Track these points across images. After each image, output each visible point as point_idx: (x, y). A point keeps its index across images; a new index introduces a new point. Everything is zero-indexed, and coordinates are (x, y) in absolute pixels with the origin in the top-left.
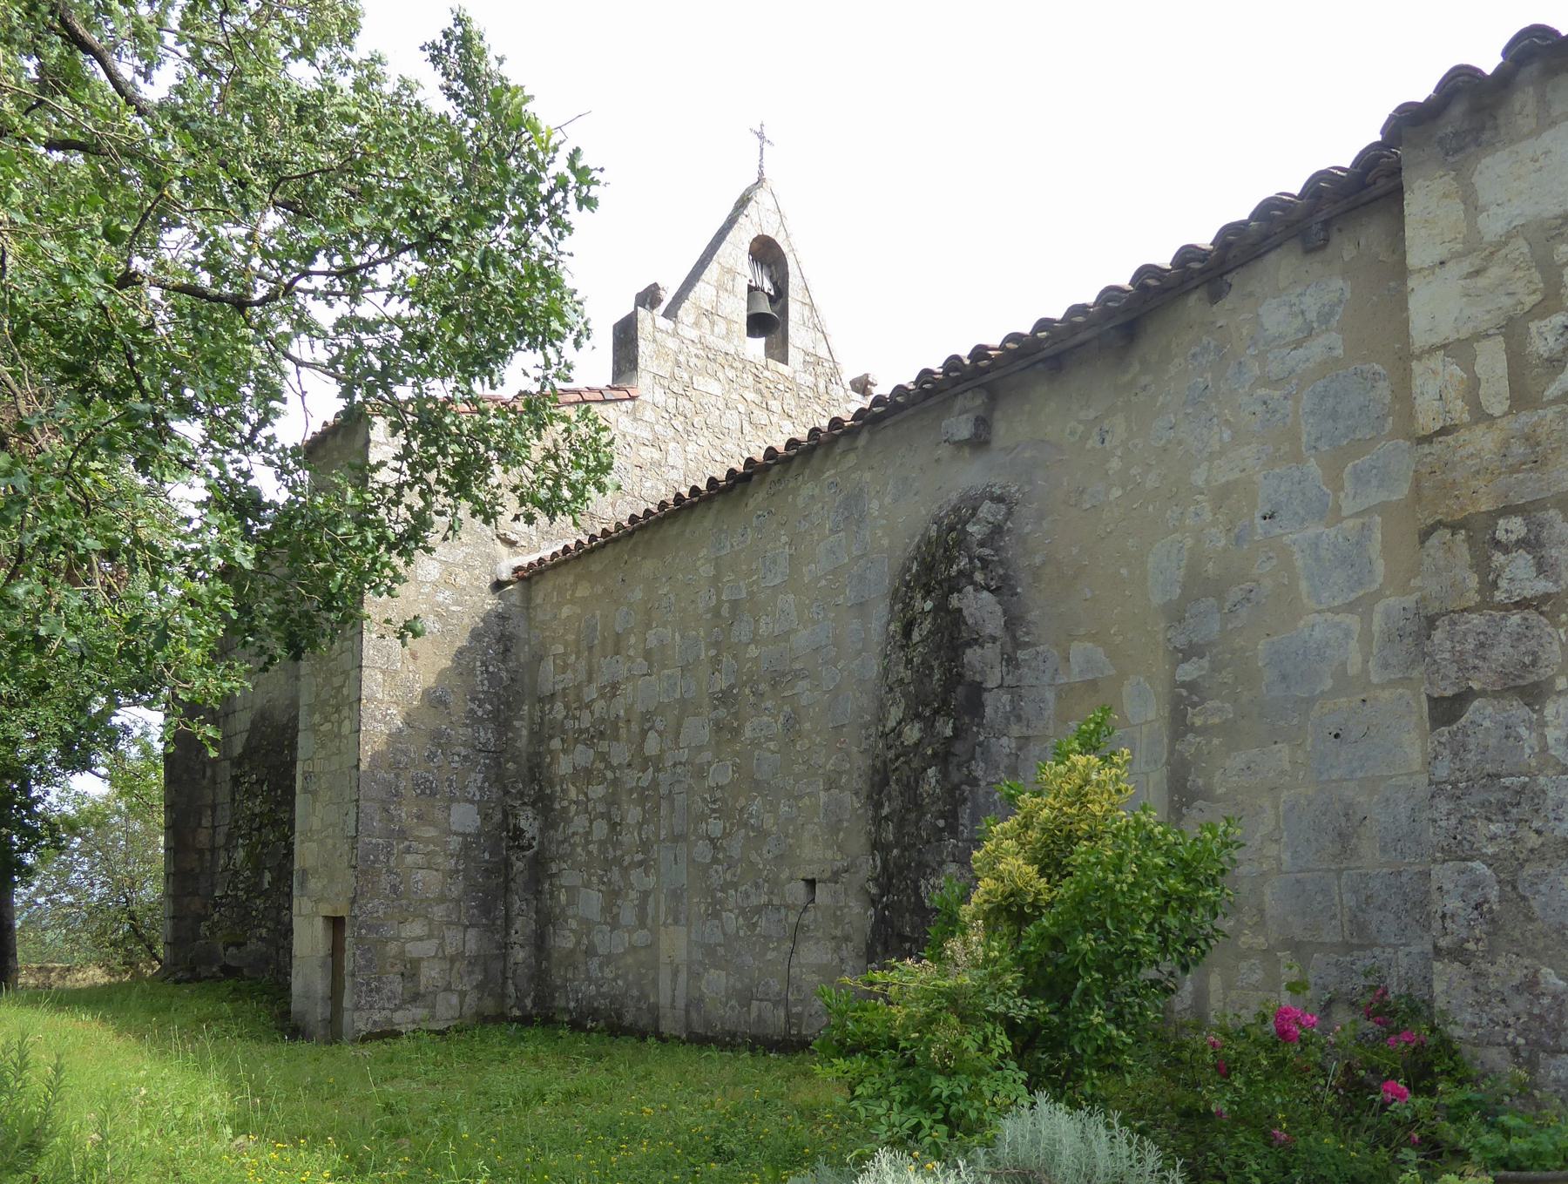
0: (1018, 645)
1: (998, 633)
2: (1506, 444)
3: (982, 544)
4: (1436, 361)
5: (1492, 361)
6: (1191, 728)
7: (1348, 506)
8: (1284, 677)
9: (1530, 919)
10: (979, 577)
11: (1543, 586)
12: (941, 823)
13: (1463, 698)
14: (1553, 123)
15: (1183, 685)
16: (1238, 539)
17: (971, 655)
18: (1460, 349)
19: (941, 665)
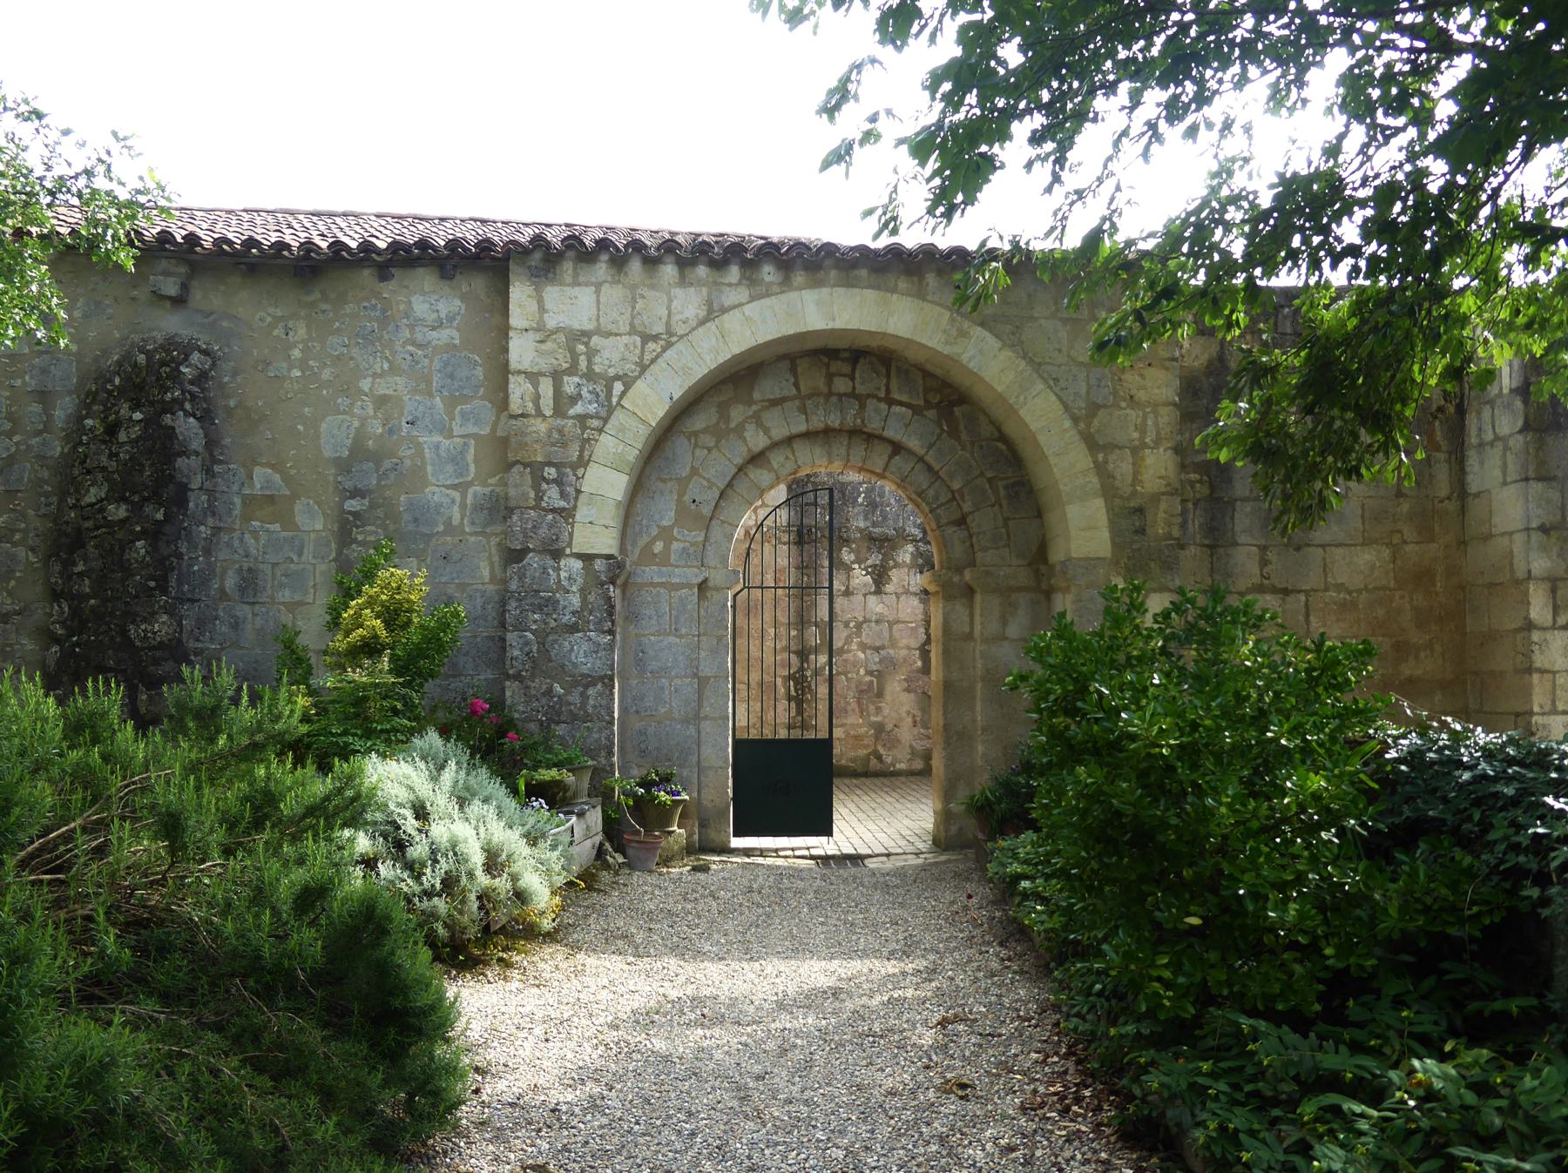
0: (215, 461)
1: (200, 449)
2: (550, 431)
3: (192, 382)
4: (521, 378)
5: (546, 388)
6: (355, 541)
7: (457, 430)
8: (416, 520)
9: (550, 661)
10: (188, 406)
11: (562, 504)
12: (152, 584)
13: (525, 551)
14: (579, 285)
15: (350, 513)
16: (391, 431)
17: (181, 462)
18: (533, 377)
19: (152, 465)
